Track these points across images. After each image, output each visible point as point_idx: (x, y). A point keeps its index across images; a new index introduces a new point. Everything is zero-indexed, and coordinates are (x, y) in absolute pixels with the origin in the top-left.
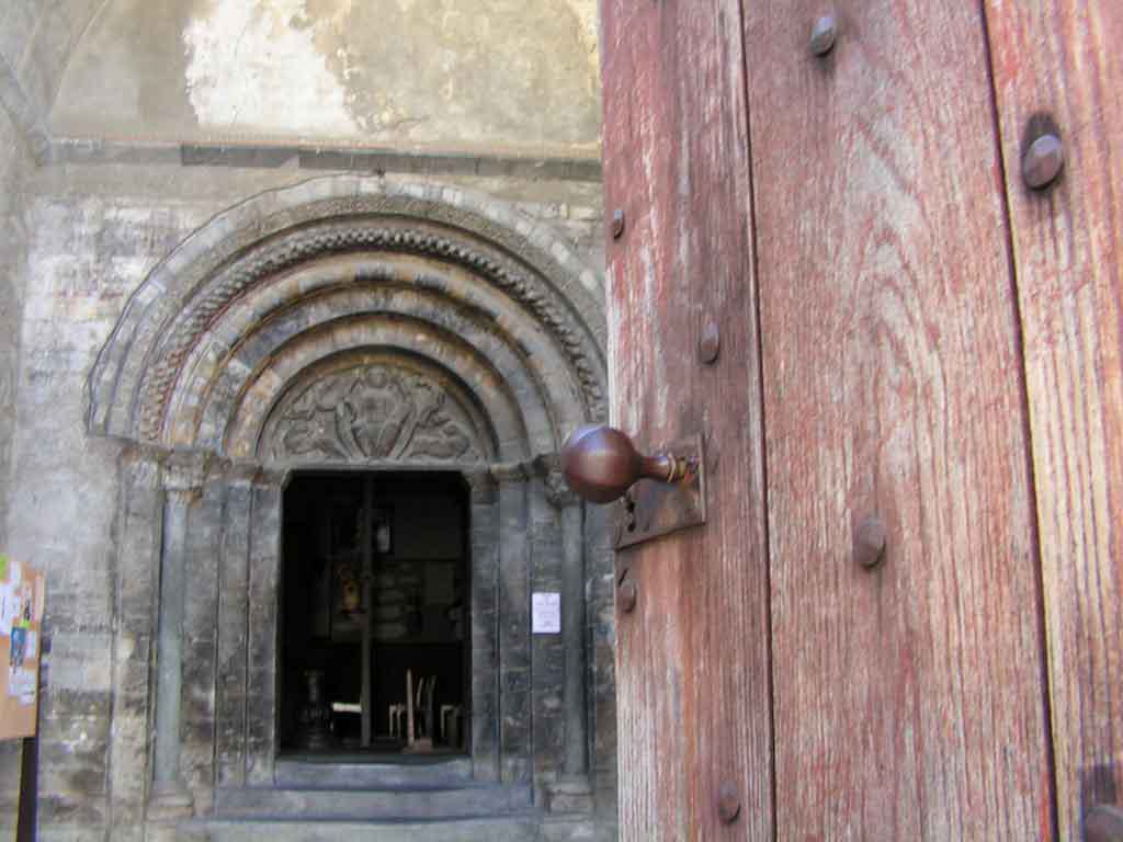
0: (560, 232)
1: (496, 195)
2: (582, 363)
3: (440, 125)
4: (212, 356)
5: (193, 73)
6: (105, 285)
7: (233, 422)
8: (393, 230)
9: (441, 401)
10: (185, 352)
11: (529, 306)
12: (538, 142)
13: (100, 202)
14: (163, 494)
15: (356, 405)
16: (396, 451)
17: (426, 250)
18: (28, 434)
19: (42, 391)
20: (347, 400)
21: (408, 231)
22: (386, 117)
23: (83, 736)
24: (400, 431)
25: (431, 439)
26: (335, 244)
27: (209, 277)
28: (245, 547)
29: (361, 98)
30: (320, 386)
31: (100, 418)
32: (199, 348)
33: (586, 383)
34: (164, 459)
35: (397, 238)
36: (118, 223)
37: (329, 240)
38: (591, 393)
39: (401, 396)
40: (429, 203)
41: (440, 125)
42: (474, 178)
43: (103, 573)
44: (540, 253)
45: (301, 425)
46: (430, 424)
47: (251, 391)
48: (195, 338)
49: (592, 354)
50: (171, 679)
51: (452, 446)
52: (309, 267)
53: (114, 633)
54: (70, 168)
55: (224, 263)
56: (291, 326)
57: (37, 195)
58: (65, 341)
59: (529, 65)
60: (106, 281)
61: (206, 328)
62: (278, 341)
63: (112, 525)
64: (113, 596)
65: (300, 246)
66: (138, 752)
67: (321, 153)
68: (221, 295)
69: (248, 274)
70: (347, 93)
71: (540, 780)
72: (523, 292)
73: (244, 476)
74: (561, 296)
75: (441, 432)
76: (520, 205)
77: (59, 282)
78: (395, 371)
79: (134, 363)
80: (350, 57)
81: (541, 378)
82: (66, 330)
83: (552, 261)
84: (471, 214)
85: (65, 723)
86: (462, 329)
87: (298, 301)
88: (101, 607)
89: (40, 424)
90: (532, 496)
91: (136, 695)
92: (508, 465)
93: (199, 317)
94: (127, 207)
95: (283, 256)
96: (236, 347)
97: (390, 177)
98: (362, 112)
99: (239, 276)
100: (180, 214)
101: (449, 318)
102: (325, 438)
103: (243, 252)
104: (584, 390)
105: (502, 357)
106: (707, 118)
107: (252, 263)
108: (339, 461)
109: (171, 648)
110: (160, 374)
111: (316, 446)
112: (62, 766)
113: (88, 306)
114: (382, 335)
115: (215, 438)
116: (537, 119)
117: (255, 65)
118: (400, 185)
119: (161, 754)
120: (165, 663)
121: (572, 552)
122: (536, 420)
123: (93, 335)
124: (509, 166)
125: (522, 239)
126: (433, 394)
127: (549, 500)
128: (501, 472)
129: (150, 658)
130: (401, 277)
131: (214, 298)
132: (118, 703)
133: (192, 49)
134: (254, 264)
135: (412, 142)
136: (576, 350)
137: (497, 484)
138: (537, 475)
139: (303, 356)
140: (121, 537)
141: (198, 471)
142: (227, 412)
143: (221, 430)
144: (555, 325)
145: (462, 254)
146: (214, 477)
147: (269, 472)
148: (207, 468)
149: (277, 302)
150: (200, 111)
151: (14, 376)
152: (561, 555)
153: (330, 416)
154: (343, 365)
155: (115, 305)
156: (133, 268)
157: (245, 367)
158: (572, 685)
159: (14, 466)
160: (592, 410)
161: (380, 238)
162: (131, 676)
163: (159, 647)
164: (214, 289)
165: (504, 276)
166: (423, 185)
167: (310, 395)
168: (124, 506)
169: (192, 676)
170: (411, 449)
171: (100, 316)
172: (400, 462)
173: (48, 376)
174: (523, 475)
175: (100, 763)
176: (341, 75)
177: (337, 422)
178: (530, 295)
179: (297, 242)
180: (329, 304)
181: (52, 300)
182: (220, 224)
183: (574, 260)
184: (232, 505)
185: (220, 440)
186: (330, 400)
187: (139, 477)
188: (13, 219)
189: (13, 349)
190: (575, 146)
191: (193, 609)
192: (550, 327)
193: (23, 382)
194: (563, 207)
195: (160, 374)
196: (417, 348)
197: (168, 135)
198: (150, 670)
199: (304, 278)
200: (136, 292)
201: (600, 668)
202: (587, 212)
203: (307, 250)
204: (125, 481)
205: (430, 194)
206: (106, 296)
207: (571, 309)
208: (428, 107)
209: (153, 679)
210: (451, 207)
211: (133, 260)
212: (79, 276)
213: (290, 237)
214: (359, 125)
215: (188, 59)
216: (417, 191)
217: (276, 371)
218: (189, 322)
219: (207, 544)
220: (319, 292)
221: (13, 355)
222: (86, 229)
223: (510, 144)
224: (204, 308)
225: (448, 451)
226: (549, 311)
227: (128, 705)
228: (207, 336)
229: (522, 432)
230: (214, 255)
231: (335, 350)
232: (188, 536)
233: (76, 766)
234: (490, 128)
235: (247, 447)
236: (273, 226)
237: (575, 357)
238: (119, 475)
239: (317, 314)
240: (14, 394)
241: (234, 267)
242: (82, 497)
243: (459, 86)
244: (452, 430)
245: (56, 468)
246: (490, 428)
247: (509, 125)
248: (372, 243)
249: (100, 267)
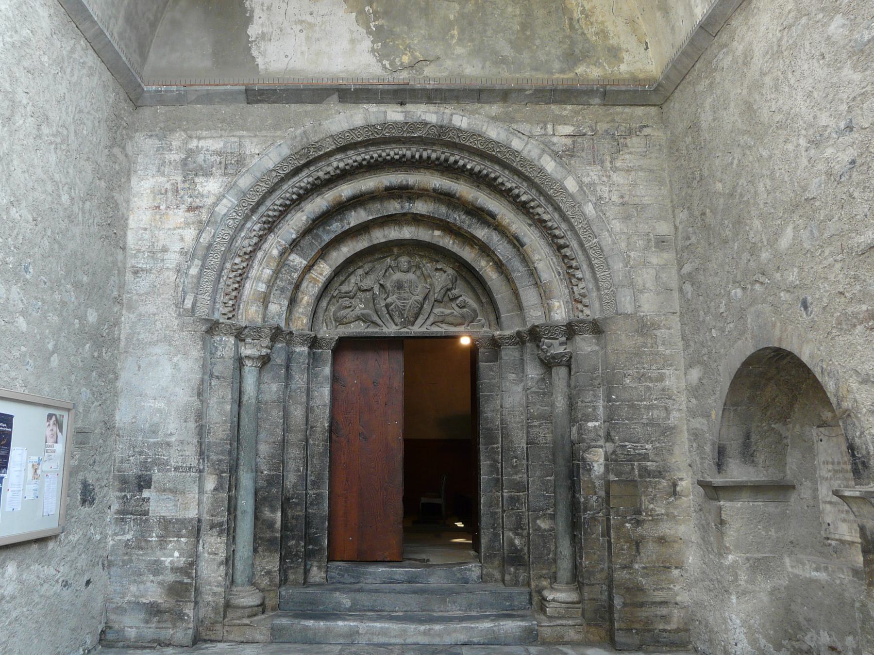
0: (548, 147)
1: (495, 119)
2: (567, 252)
3: (449, 63)
4: (275, 252)
5: (253, 31)
6: (190, 200)
7: (293, 301)
9: (454, 282)
10: (255, 250)
11: (523, 208)
12: (527, 74)
13: (184, 135)
14: (240, 362)
15: (388, 285)
17: (441, 164)
18: (132, 317)
19: (143, 284)
20: (381, 282)
21: (425, 150)
22: (406, 59)
23: (177, 554)
24: (422, 306)
25: (447, 311)
26: (369, 162)
27: (271, 191)
28: (304, 399)
29: (384, 45)
30: (360, 272)
31: (188, 304)
32: (266, 246)
33: (571, 267)
34: (240, 335)
35: (417, 156)
36: (198, 150)
37: (364, 159)
38: (574, 276)
39: (422, 277)
40: (441, 127)
41: (449, 63)
42: (477, 106)
43: (192, 425)
44: (532, 164)
45: (346, 302)
46: (446, 299)
47: (307, 276)
48: (262, 238)
49: (574, 244)
50: (246, 503)
51: (463, 317)
52: (348, 181)
53: (200, 471)
54: (160, 109)
55: (283, 180)
56: (336, 227)
57: (136, 131)
58: (161, 243)
59: (518, 12)
60: (191, 197)
61: (270, 230)
62: (327, 238)
63: (199, 389)
64: (200, 444)
65: (341, 165)
66: (221, 563)
67: (356, 90)
68: (281, 205)
69: (301, 188)
70: (373, 42)
71: (537, 586)
72: (518, 196)
73: (303, 344)
74: (549, 199)
75: (454, 305)
76: (514, 126)
77: (154, 199)
78: (418, 259)
79: (214, 260)
80: (375, 13)
81: (533, 263)
82: (161, 235)
83: (541, 170)
84: (475, 135)
85: (163, 541)
86: (469, 226)
87: (340, 208)
88: (191, 452)
89: (142, 309)
90: (527, 357)
91: (219, 519)
92: (507, 333)
93: (264, 223)
94: (205, 138)
95: (328, 173)
96: (294, 245)
97: (410, 107)
98: (386, 56)
99: (295, 190)
100: (247, 142)
101: (458, 218)
102: (364, 312)
103: (297, 171)
104: (568, 273)
105: (502, 249)
106: (849, 62)
107: (304, 179)
108: (377, 330)
109: (246, 480)
110: (236, 267)
111: (358, 318)
112: (160, 578)
113: (179, 216)
114: (407, 233)
115: (280, 315)
116: (526, 56)
117: (301, 22)
118: (419, 113)
119: (239, 566)
120: (242, 492)
121: (560, 403)
122: (530, 296)
123: (182, 239)
124: (504, 95)
125: (516, 153)
126: (448, 275)
127: (541, 360)
128: (502, 337)
129: (230, 490)
130: (421, 186)
131: (276, 207)
132: (204, 526)
133: (252, 11)
134: (305, 180)
135: (426, 78)
136: (561, 242)
137: (499, 347)
138: (531, 341)
139: (346, 250)
140: (206, 395)
141: (266, 342)
142: (289, 294)
143: (284, 308)
144: (545, 221)
145: (469, 167)
146: (280, 345)
147: (323, 339)
148: (274, 338)
149: (325, 208)
150: (260, 61)
151: (121, 273)
152: (552, 405)
154: (377, 256)
155: (199, 215)
156: (211, 186)
157: (301, 260)
158: (563, 509)
159: (122, 344)
160: (575, 288)
161: (404, 156)
162: (216, 502)
163: (237, 479)
164: (276, 201)
165: (503, 184)
166: (436, 113)
167: (353, 279)
168: (208, 373)
169: (259, 502)
170: (431, 320)
171: (187, 224)
172: (423, 329)
173: (149, 271)
174: (519, 340)
175: (189, 575)
176: (368, 27)
177: (374, 300)
178: (524, 198)
179: (338, 162)
180: (365, 209)
181: (149, 213)
182: (279, 148)
183: (560, 169)
184: (294, 365)
185: (284, 315)
186: (367, 283)
187: (220, 348)
188: (116, 150)
189: (120, 252)
190: (557, 76)
191: (264, 449)
192: (540, 223)
193: (129, 276)
194: (549, 127)
195: (236, 267)
196: (434, 241)
197: (236, 82)
198: (230, 498)
199: (346, 190)
200: (215, 204)
201: (586, 499)
202: (568, 129)
203: (347, 167)
204: (209, 351)
205: (443, 120)
206: (191, 209)
207: (557, 208)
208: (438, 51)
209: (232, 508)
210: (459, 130)
211: (211, 179)
212: (170, 194)
213: (332, 159)
214: (384, 67)
215: (249, 21)
216: (432, 118)
217: (325, 261)
218: (256, 227)
219: (275, 397)
220: (358, 201)
221: (120, 257)
222: (175, 157)
223: (504, 76)
224: (269, 216)
225: (459, 321)
226: (540, 210)
227: (212, 527)
228: (271, 238)
230: (274, 174)
231: (370, 244)
232: (259, 391)
233: (170, 578)
234: (488, 64)
235: (305, 321)
236: (319, 149)
237: (560, 247)
238: (204, 347)
239: (356, 217)
240: (122, 286)
241: (290, 183)
242: (175, 366)
243: (462, 31)
244: (463, 304)
245: (154, 343)
246: (493, 302)
247: (504, 61)
248: (397, 160)
249: (187, 185)
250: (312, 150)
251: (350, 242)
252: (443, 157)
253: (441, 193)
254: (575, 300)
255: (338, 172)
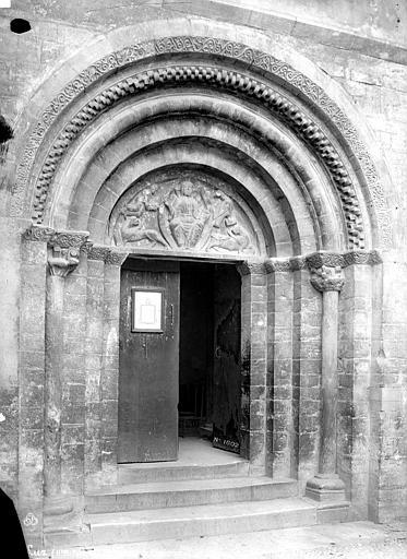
8: (225, 72)
11: (313, 145)
16: (199, 245)
26: (174, 78)
144: (332, 159)
153: (154, 215)
165: (300, 119)
186: (153, 204)
199: (152, 103)
203: (161, 79)
220: (164, 116)
226: (328, 149)
229: (295, 238)
230: (94, 71)
239: (159, 134)
250: (133, 52)
251: (144, 160)
252: (250, 85)
253: (239, 122)
254: (351, 234)
255: (152, 82)
